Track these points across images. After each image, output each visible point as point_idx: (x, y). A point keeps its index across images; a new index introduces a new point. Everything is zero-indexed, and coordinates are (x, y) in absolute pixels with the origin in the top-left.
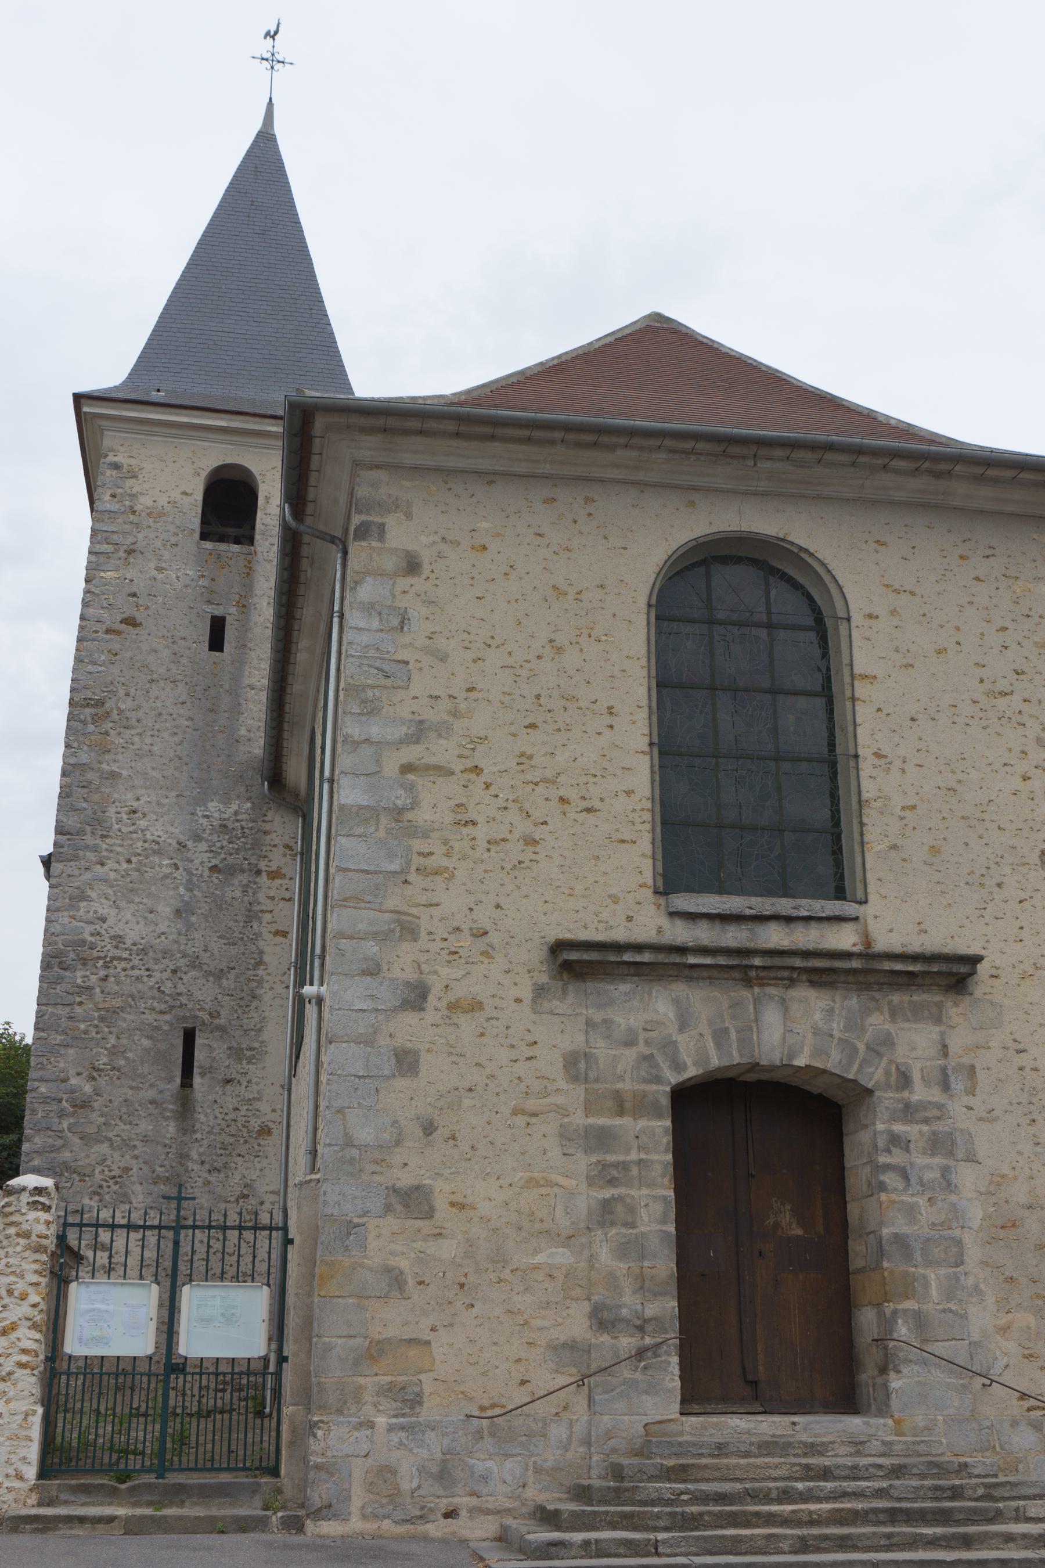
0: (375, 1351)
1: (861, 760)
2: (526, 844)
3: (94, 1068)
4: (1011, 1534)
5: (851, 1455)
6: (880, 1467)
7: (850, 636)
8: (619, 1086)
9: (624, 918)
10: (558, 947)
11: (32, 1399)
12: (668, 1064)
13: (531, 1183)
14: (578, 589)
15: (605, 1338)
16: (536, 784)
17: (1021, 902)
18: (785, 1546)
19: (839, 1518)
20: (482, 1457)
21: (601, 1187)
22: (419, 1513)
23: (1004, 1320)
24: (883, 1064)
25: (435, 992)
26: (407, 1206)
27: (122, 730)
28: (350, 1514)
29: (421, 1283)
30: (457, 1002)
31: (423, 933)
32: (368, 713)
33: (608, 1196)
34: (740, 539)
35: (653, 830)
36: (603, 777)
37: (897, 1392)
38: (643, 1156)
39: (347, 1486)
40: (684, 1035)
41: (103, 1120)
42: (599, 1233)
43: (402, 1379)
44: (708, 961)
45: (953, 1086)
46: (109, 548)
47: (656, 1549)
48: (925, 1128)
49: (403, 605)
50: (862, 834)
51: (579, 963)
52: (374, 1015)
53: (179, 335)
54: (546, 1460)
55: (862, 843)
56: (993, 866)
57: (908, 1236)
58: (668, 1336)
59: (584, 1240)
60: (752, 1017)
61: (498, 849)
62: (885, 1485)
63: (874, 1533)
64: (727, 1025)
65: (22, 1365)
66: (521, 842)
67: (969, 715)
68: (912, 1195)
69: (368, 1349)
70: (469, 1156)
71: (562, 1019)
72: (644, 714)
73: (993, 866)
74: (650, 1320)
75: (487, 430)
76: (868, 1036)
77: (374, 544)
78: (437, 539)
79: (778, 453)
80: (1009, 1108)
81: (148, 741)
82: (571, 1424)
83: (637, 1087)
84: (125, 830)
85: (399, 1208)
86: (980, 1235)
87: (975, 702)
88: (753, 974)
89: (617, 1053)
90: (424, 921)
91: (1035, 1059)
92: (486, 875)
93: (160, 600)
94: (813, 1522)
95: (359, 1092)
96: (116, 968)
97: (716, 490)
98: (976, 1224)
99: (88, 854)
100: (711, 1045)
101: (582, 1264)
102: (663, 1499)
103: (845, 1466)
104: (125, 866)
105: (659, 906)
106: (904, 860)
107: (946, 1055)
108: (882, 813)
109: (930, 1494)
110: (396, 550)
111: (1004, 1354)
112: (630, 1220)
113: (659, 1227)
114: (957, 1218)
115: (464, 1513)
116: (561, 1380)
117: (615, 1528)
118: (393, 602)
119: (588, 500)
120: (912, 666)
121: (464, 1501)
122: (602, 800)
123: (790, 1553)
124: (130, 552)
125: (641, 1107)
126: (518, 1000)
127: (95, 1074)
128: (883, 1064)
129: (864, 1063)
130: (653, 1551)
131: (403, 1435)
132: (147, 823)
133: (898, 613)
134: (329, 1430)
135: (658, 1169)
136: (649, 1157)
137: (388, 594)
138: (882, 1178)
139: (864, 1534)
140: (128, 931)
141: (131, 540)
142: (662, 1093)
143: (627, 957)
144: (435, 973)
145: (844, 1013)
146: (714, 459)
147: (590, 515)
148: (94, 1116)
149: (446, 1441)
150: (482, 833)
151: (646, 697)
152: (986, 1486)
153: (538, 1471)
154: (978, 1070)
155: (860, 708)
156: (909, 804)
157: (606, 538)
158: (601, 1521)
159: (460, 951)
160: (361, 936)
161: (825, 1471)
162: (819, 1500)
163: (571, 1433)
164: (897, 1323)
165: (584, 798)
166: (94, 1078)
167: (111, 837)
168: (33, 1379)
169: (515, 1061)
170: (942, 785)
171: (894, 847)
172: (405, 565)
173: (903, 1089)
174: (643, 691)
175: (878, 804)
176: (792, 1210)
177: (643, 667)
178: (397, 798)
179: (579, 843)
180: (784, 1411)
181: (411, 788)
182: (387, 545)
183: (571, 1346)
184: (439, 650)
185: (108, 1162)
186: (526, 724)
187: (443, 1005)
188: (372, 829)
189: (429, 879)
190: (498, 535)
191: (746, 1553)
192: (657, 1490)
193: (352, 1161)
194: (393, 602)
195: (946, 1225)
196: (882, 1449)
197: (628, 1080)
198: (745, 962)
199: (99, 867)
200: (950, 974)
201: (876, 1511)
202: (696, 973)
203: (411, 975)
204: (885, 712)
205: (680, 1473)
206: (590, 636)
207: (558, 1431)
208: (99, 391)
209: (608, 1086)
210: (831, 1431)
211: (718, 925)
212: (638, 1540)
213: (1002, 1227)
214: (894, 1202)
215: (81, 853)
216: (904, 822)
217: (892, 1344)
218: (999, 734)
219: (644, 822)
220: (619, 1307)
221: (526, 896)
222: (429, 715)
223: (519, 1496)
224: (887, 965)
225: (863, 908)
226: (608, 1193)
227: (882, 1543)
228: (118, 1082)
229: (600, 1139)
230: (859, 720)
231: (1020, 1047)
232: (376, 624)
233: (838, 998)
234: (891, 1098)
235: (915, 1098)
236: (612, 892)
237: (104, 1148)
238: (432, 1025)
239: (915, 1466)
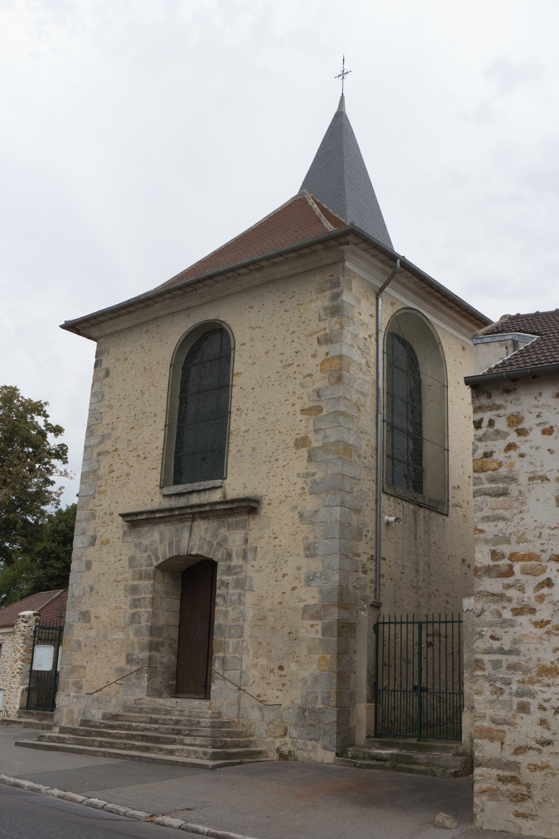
0: (73, 669)
6: (172, 720)
11: (19, 684)
15: (129, 667)
16: (131, 451)
19: (128, 737)
25: (98, 538)
43: (78, 680)
45: (248, 557)
48: (235, 577)
51: (135, 521)
56: (275, 451)
65: (18, 673)
73: (275, 451)
78: (115, 360)
82: (117, 698)
98: (250, 618)
106: (242, 456)
120: (255, 363)
162: (138, 730)
168: (20, 677)
175: (235, 432)
195: (237, 620)
222: (106, 432)
231: (275, 536)
233: (210, 523)
235: (233, 564)
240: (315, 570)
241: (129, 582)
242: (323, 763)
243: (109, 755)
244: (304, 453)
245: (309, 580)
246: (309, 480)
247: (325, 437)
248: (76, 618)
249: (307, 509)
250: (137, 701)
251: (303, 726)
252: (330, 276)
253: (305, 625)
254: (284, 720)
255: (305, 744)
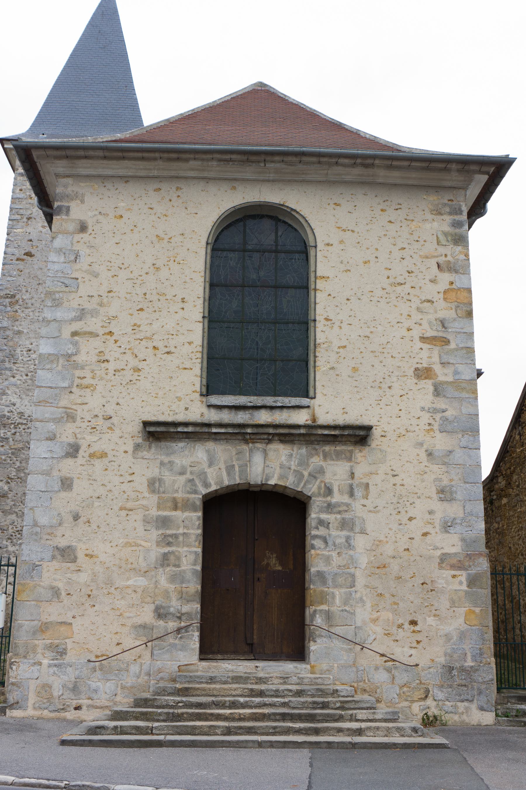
0: (44, 628)
1: (317, 323)
2: (134, 371)
3: (9, 478)
4: (341, 728)
5: (281, 684)
6: (290, 691)
7: (316, 256)
8: (176, 495)
9: (184, 408)
10: (146, 424)
12: (201, 483)
13: (128, 544)
14: (169, 237)
15: (161, 623)
16: (141, 340)
17: (401, 396)
18: (218, 731)
20: (95, 680)
21: (163, 547)
22: (62, 707)
23: (375, 616)
24: (317, 483)
26: (63, 556)
27: (24, 309)
28: (27, 707)
29: (69, 594)
30: (94, 453)
31: (78, 418)
32: (56, 306)
33: (166, 551)
34: (260, 205)
35: (202, 362)
36: (177, 335)
37: (313, 652)
38: (186, 531)
39: (27, 693)
40: (212, 469)
41: (13, 503)
42: (161, 570)
43: (57, 641)
44: (223, 430)
45: (356, 494)
46: (19, 217)
47: (152, 731)
48: (339, 516)
49: (77, 249)
50: (315, 362)
51: (157, 433)
52: (51, 460)
53: (57, 104)
54: (127, 683)
55: (315, 367)
56: (387, 377)
57: (325, 572)
58: (193, 622)
59: (153, 573)
60: (248, 459)
61: (120, 374)
62: (287, 701)
63: (267, 726)
64: (234, 463)
66: (132, 370)
67: (380, 296)
68: (329, 551)
69: (40, 627)
70: (96, 531)
71: (148, 461)
72: (201, 301)
73: (387, 377)
74: (184, 614)
75: (120, 154)
76: (311, 468)
77: (64, 217)
78: (97, 213)
79: (277, 158)
80: (386, 506)
81: (37, 314)
83: (185, 496)
84: (25, 359)
85: (59, 557)
86: (365, 572)
87: (383, 289)
88: (248, 437)
89: (175, 478)
90: (79, 414)
91: (403, 480)
92: (112, 388)
93: (44, 242)
94: (241, 719)
95: (42, 499)
96: (20, 428)
97: (248, 180)
98: (363, 566)
99: (7, 372)
100: (225, 474)
101: (152, 585)
102: (169, 705)
103: (272, 690)
104: (25, 377)
105: (202, 402)
106: (337, 375)
107: (353, 478)
108: (327, 350)
109: (310, 706)
110: (75, 220)
111: (374, 634)
112: (177, 563)
113: (192, 567)
114: (353, 563)
115: (84, 708)
116: (138, 643)
117: (137, 720)
118: (72, 247)
119: (178, 189)
120: (349, 271)
121: (84, 702)
122: (175, 347)
123: (221, 735)
124: (29, 219)
125: (187, 506)
126: (126, 452)
127: (9, 481)
128: (317, 483)
129: (307, 482)
130: (150, 732)
131: (55, 669)
132: (36, 356)
133: (344, 242)
134: (19, 666)
135: (193, 537)
136: (189, 531)
137: (70, 243)
138: (313, 542)
139: (261, 727)
140: (26, 410)
141: (30, 212)
142: (197, 499)
143: (180, 429)
144: (84, 438)
145: (298, 457)
146: (242, 163)
147: (179, 196)
148: (9, 501)
149: (77, 672)
150: (111, 366)
151: (203, 292)
152: (341, 702)
153: (123, 688)
154: (370, 486)
155: (318, 294)
156: (343, 345)
157: (186, 208)
158: (130, 716)
159: (97, 427)
160: (46, 420)
161: (261, 692)
162: (251, 707)
163: (141, 669)
164: (316, 616)
165: (166, 347)
166: (9, 483)
167: (18, 363)
169: (122, 483)
170: (362, 334)
171: (332, 368)
172: (79, 228)
173: (327, 496)
174: (201, 289)
175: (325, 345)
176: (276, 557)
177: (202, 277)
178: (69, 349)
179: (162, 370)
180: (265, 659)
181: (76, 344)
182: (70, 218)
183: (144, 626)
184: (94, 272)
185: (15, 524)
186: (138, 309)
187: (87, 454)
188: (55, 366)
189: (83, 391)
190: (129, 209)
191: (198, 734)
192: (166, 700)
193: (36, 534)
194: (72, 247)
196: (297, 681)
197: (180, 492)
198: (243, 431)
199: (12, 378)
200: (356, 436)
201: (275, 714)
202: (218, 437)
203: (71, 440)
204: (333, 296)
205: (185, 692)
206: (174, 261)
207: (134, 669)
208: (13, 136)
209: (170, 495)
210: (276, 671)
211: (233, 411)
212: (143, 727)
213: (378, 568)
214: (318, 555)
215: (3, 372)
216: (340, 355)
217: (312, 627)
218: (396, 306)
219: (197, 358)
220: (169, 607)
221: (133, 398)
222: (87, 306)
223: (113, 700)
224: (320, 432)
225: (313, 401)
226: (166, 550)
227: (270, 731)
228: (20, 484)
229: (164, 522)
230: (317, 301)
231: (395, 473)
232: (62, 259)
234: (320, 501)
235: (334, 500)
236: (178, 395)
237: (14, 517)
238: (81, 465)
239: (309, 691)
240: (453, 515)
241: (150, 512)
242: (480, 725)
243: (269, 744)
244: (428, 385)
245: (447, 526)
246: (438, 416)
247: (456, 373)
248: (47, 555)
249: (437, 448)
250: (183, 668)
251: (451, 686)
252: (449, 200)
253: (444, 576)
254: (423, 682)
255: (456, 707)
